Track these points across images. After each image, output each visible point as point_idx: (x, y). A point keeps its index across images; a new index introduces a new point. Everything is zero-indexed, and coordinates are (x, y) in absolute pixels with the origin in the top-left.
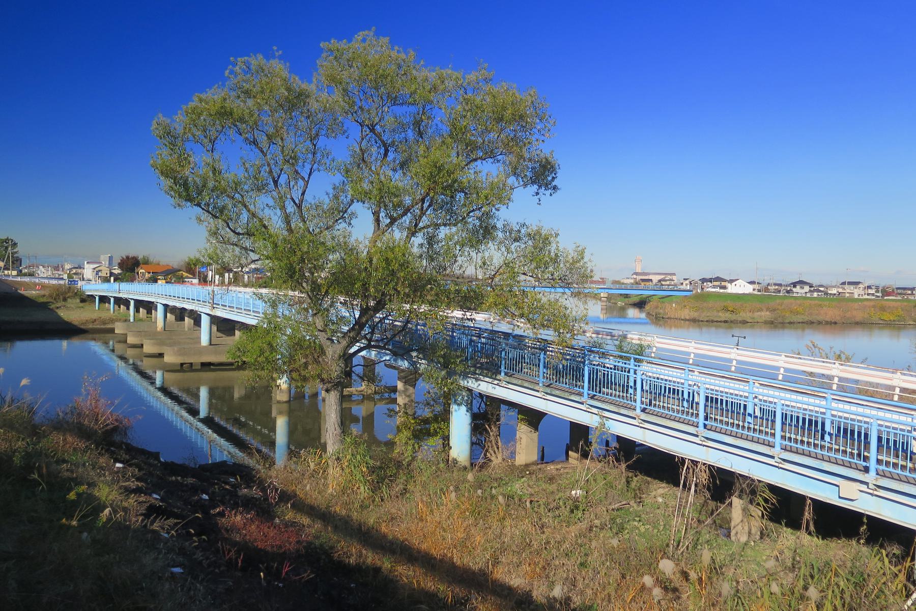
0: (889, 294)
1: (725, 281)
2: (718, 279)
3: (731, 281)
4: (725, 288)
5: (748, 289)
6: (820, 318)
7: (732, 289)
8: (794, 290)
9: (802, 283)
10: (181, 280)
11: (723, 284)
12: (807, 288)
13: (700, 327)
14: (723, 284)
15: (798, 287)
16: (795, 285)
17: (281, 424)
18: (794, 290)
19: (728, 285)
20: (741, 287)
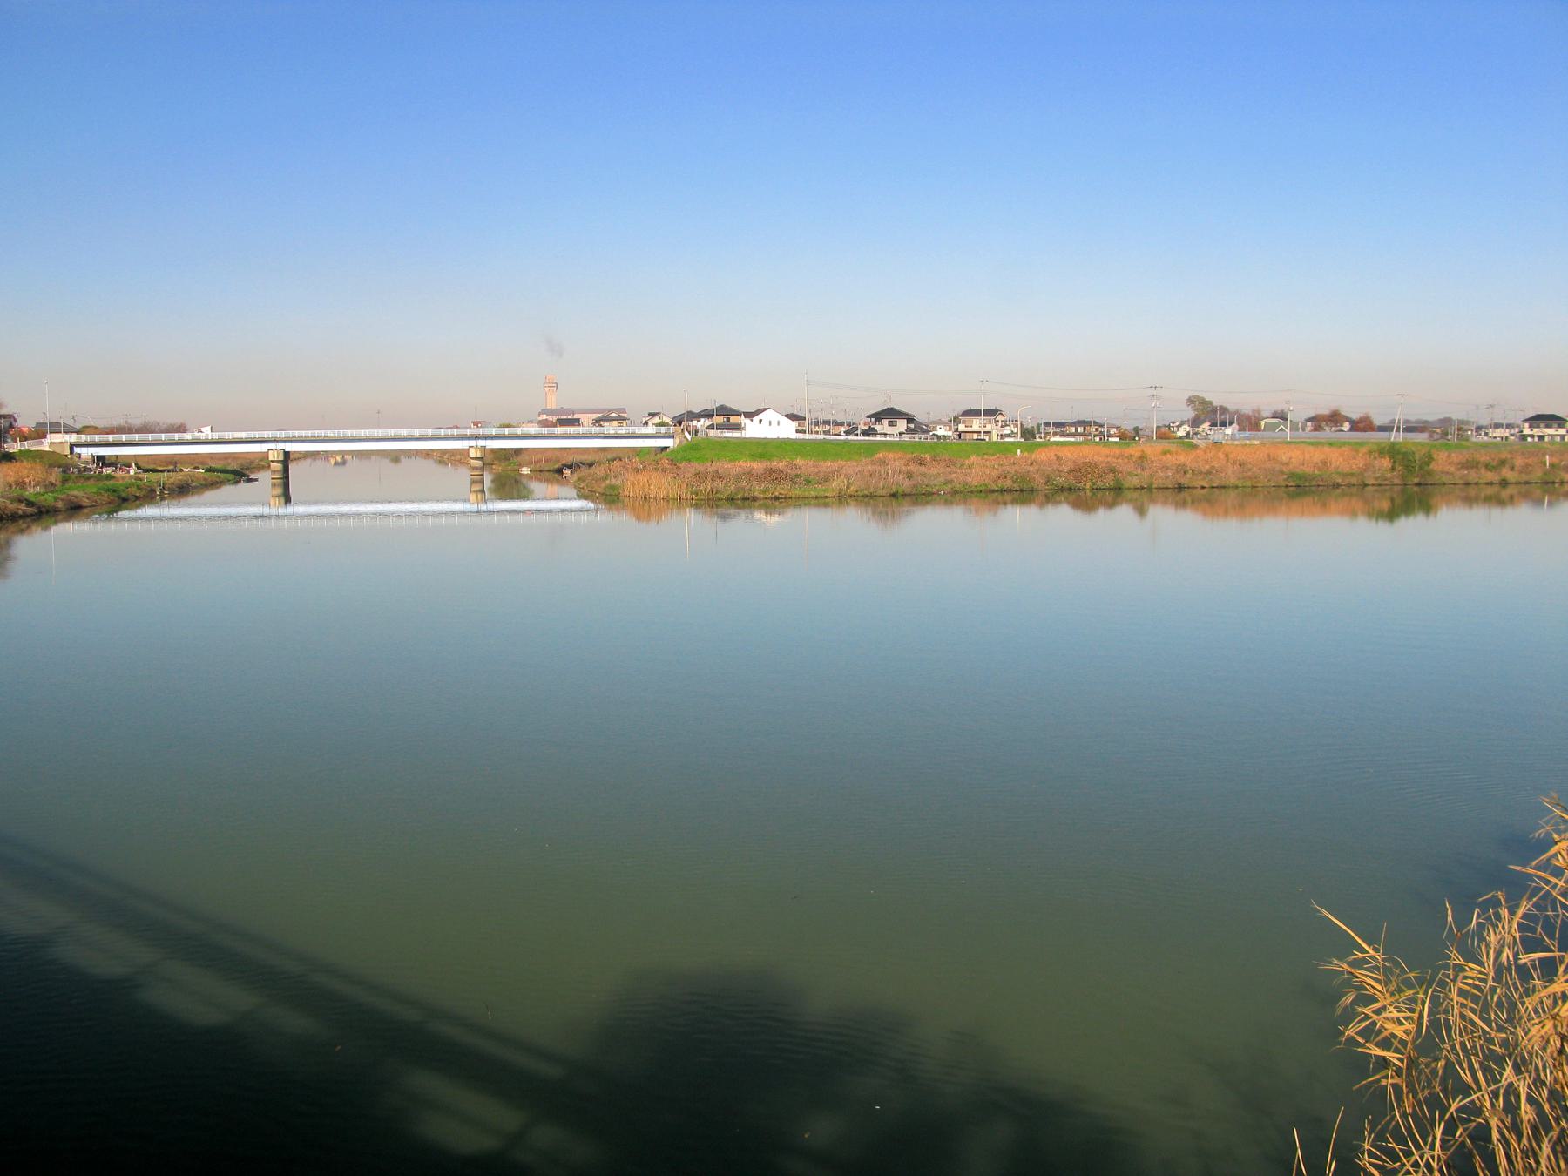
0: (105, 465)
1: (738, 414)
2: (724, 411)
3: (750, 415)
4: (738, 428)
5: (788, 430)
6: (957, 478)
7: (753, 430)
8: (878, 428)
9: (891, 414)
10: (645, 507)
11: (734, 420)
12: (902, 425)
13: (826, 505)
14: (734, 420)
15: (885, 422)
16: (878, 417)
17: (1450, 918)
18: (878, 428)
19: (744, 421)
20: (773, 427)
